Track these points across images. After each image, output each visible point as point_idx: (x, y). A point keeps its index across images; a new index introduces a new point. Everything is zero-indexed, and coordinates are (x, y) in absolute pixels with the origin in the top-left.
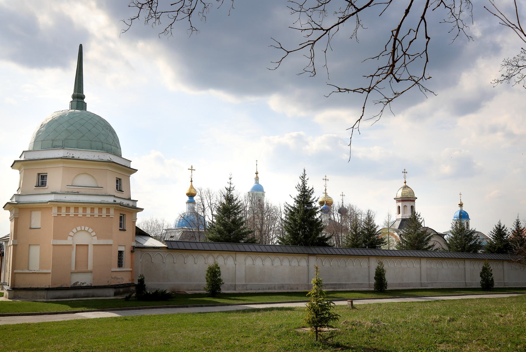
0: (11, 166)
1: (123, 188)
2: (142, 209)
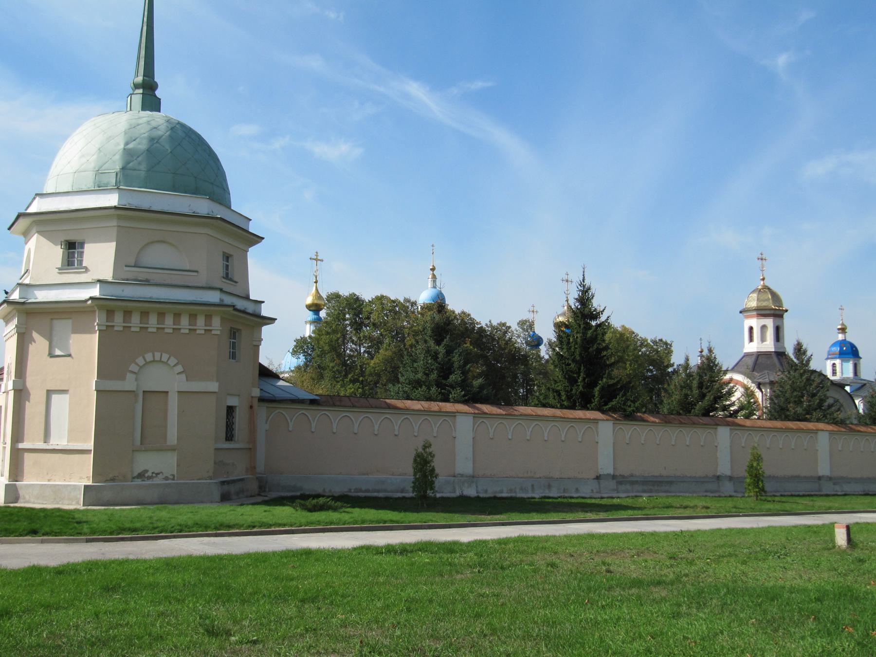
0: (8, 226)
2: (272, 320)
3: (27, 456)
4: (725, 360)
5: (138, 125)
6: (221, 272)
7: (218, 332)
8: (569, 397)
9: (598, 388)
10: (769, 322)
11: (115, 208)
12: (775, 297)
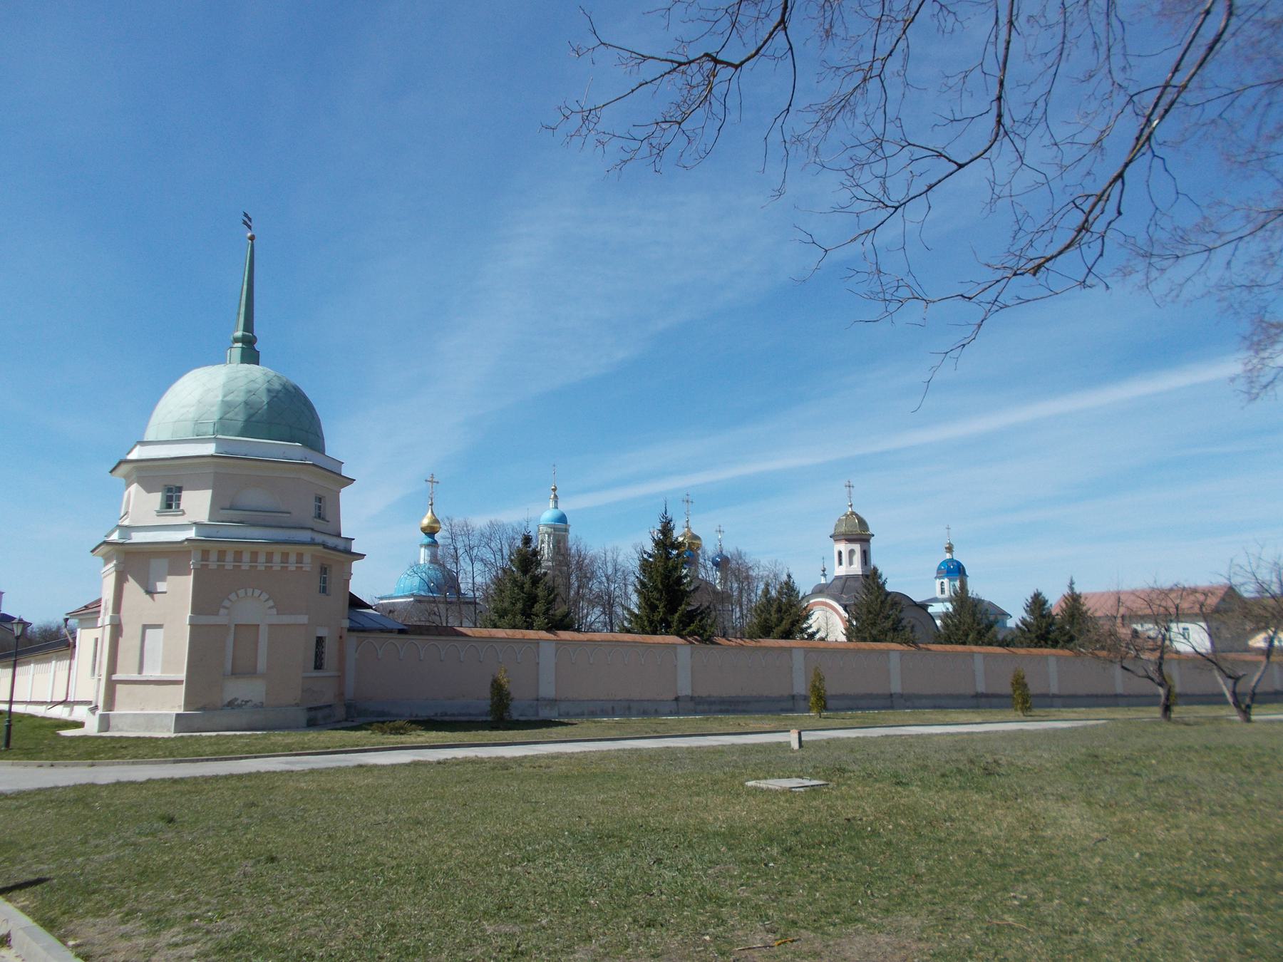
0: (110, 469)
1: (328, 515)
2: (361, 556)
3: (119, 687)
4: (804, 586)
5: (236, 378)
6: (313, 512)
7: (308, 569)
8: (651, 622)
9: (677, 615)
10: (857, 547)
11: (212, 456)
12: (862, 523)
